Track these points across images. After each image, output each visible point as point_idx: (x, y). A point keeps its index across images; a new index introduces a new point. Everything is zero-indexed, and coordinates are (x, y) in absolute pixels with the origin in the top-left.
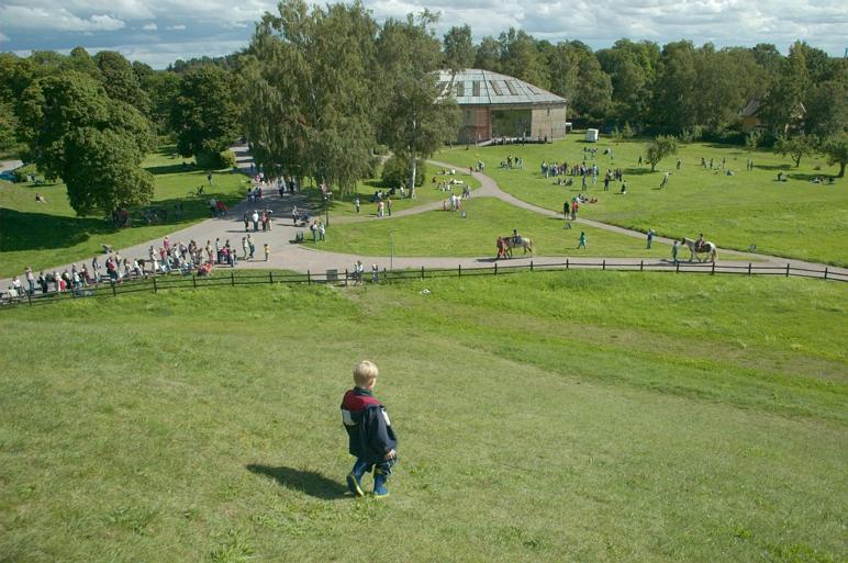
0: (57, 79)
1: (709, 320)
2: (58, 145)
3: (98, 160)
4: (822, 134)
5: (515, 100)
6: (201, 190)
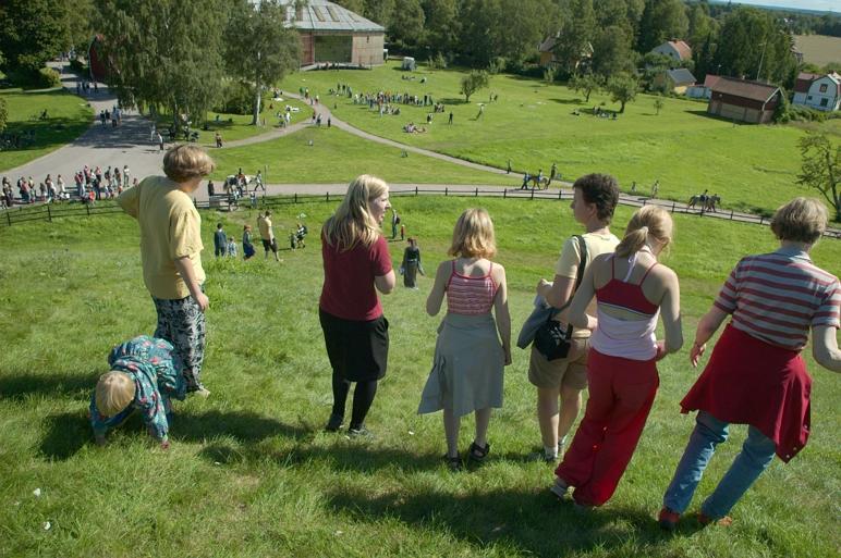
1: (537, 238)
4: (607, 73)
5: (337, 26)
6: (45, 114)
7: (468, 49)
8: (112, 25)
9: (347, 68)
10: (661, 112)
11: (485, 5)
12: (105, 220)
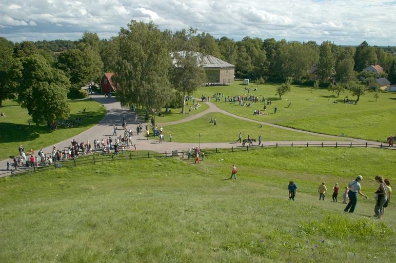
0: (29, 58)
2: (29, 91)
3: (50, 98)
5: (212, 66)
6: (84, 110)
7: (273, 74)
8: (119, 67)
9: (218, 85)
10: (378, 99)
11: (282, 53)
12: (121, 163)
